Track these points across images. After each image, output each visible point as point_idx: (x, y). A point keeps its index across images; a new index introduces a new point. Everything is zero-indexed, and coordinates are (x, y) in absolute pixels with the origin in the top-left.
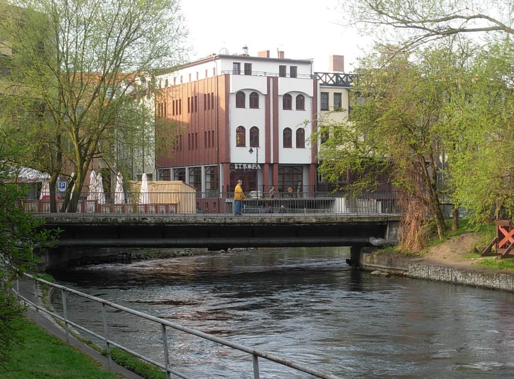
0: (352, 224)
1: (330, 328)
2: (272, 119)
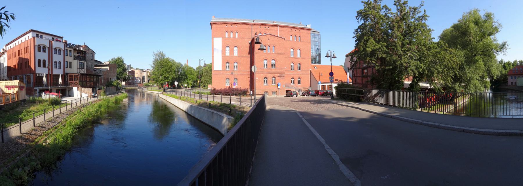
1: (433, 108)
2: (50, 57)
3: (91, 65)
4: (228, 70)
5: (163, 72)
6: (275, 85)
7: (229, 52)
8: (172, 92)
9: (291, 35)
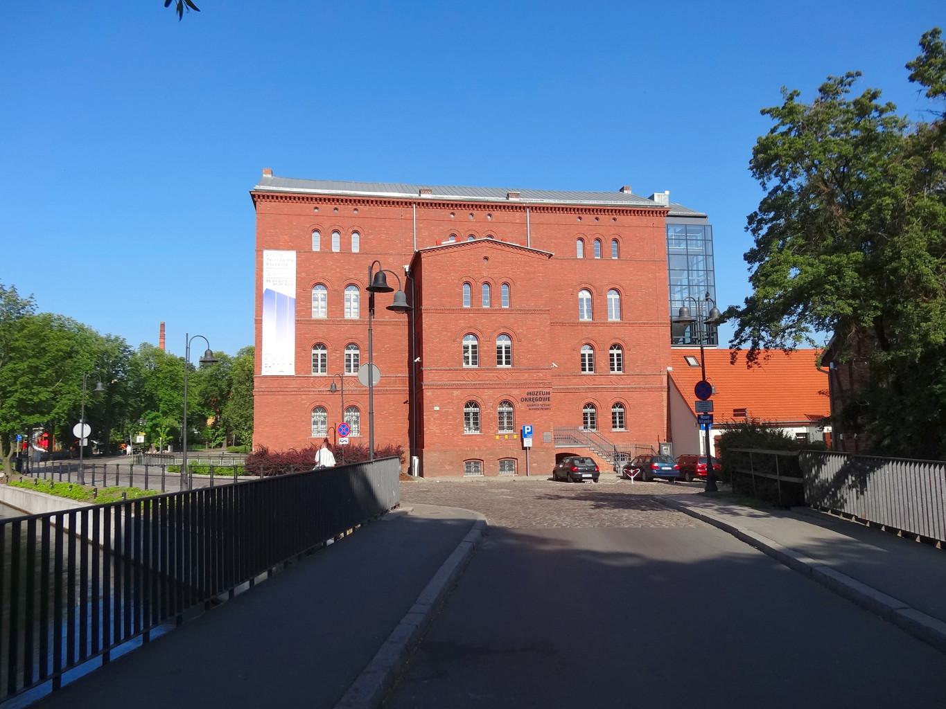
4: (319, 374)
5: (16, 378)
6: (511, 432)
7: (324, 304)
8: (62, 470)
9: (581, 239)
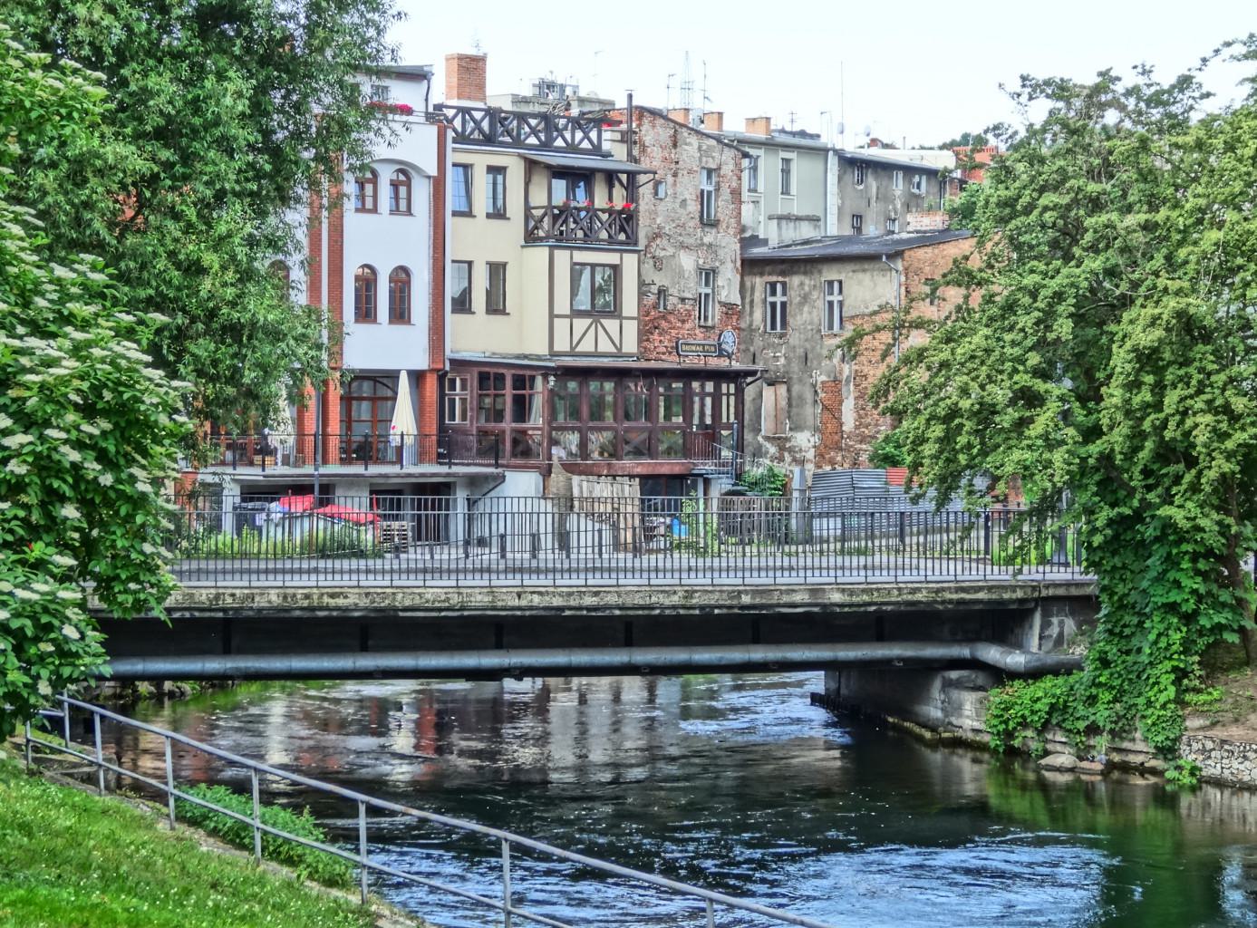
0: (941, 607)
3: (700, 270)
